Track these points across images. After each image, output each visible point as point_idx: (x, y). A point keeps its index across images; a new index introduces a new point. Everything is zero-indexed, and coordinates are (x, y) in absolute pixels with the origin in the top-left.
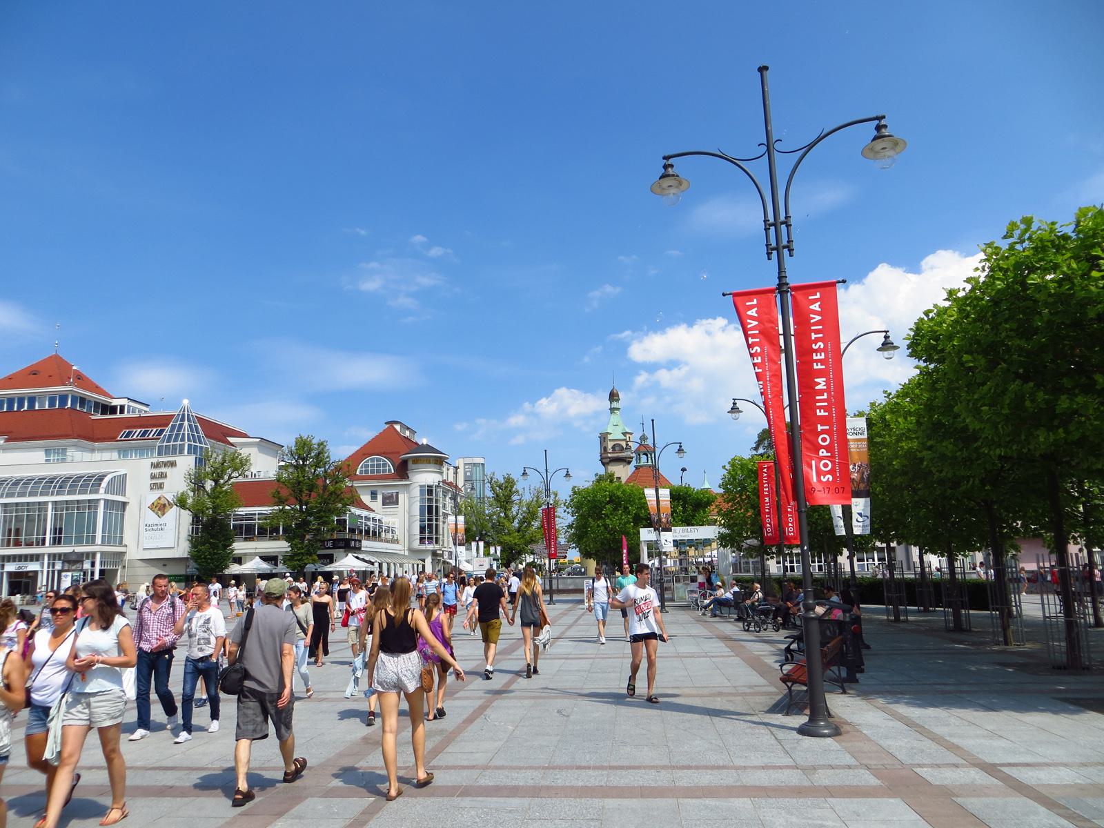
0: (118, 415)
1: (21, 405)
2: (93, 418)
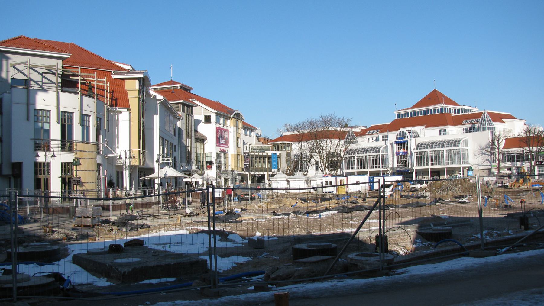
0: (460, 114)
1: (428, 113)
2: (452, 115)
